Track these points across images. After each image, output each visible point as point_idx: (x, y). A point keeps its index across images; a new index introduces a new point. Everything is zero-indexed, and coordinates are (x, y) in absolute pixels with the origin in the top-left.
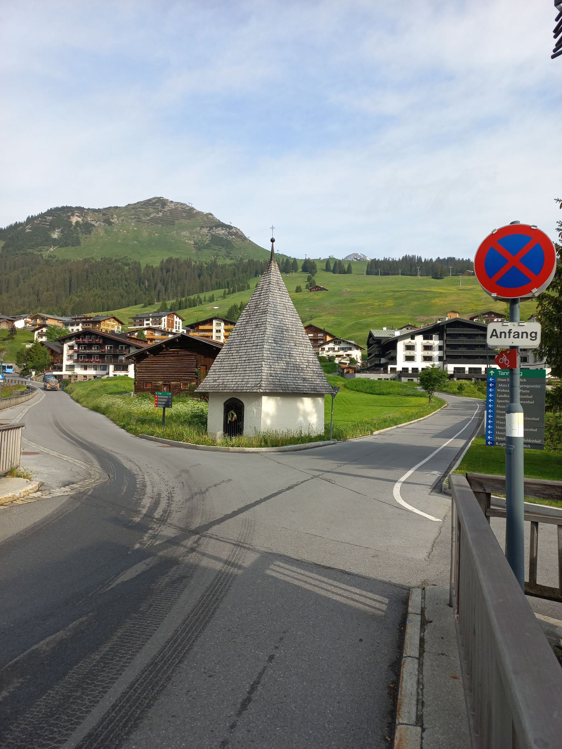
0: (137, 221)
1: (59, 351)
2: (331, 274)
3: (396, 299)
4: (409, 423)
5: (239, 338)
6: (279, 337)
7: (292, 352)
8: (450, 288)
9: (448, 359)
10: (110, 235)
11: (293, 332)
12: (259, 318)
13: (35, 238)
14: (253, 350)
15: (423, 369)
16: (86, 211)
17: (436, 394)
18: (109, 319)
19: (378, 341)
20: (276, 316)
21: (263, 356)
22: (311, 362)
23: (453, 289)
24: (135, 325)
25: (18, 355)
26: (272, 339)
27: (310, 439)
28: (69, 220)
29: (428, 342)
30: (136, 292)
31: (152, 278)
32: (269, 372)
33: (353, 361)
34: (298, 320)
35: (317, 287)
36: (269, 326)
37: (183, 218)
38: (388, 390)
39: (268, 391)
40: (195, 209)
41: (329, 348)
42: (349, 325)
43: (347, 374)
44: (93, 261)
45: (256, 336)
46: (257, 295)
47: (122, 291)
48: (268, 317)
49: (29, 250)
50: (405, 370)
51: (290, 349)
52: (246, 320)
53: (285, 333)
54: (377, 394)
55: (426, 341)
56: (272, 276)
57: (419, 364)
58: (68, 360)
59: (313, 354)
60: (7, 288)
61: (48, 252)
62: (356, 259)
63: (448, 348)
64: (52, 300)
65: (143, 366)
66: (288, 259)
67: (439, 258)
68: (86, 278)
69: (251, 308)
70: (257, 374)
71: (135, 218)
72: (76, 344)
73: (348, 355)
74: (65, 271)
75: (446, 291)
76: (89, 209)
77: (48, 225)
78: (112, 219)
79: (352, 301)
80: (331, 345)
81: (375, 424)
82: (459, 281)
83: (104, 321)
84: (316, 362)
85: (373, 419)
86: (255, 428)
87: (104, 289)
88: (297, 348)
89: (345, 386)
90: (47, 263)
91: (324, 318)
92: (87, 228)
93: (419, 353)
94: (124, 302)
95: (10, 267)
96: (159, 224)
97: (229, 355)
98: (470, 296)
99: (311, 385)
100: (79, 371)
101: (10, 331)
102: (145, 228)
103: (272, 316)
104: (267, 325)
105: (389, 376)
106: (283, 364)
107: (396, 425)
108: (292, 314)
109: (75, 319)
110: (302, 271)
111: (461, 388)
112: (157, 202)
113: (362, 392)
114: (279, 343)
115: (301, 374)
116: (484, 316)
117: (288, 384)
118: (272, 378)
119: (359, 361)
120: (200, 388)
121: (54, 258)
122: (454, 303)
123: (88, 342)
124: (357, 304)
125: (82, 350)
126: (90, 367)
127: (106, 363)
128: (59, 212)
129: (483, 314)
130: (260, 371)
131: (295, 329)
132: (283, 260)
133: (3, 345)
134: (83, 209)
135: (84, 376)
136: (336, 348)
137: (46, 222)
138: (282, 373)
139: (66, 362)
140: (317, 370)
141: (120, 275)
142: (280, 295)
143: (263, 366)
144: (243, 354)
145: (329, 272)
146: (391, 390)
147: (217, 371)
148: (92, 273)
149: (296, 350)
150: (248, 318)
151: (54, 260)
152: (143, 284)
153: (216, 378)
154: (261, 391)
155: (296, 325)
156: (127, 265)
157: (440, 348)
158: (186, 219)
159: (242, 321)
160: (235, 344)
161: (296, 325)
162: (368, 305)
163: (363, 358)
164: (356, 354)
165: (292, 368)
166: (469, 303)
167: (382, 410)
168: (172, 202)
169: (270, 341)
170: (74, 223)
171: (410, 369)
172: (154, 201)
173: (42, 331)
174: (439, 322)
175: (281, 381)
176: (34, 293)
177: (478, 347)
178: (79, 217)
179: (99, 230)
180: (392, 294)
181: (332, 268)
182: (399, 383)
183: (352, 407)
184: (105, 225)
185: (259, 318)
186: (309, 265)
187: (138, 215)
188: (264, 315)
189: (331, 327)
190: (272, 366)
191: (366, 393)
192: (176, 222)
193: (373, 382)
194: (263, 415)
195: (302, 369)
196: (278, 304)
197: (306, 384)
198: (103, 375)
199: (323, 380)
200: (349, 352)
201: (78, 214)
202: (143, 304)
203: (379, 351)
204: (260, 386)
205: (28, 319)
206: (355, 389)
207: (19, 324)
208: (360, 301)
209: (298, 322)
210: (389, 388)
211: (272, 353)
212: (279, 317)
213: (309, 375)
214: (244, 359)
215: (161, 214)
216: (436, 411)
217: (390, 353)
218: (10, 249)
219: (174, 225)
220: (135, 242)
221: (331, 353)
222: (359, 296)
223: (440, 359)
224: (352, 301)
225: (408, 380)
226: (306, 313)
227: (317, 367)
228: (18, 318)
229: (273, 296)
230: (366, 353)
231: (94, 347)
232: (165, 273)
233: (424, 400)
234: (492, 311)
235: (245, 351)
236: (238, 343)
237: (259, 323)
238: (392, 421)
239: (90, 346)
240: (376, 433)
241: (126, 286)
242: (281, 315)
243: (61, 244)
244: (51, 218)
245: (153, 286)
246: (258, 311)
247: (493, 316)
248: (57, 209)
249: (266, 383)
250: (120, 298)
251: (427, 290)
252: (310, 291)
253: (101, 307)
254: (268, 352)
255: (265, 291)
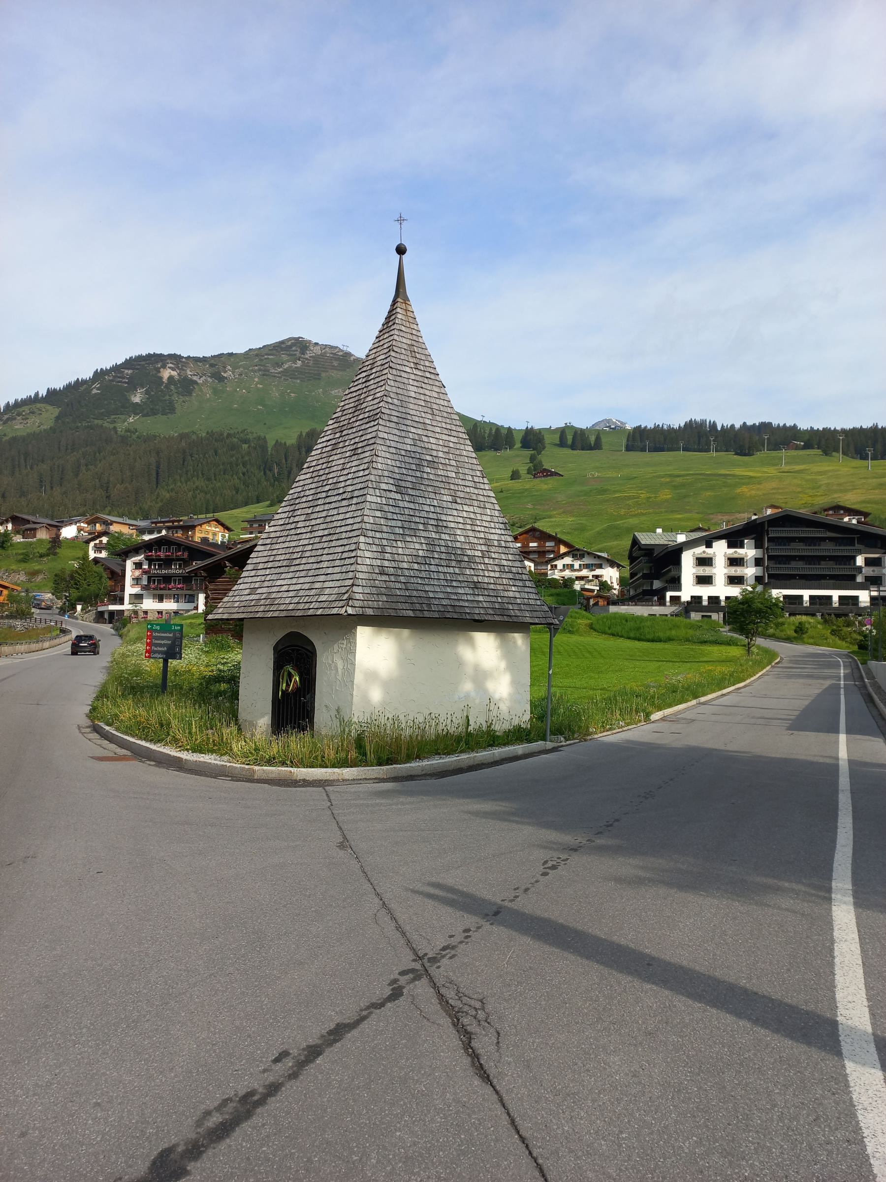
0: (264, 375)
1: (118, 570)
2: (567, 451)
3: (675, 487)
4: (720, 693)
5: (313, 486)
6: (409, 479)
7: (444, 518)
8: (765, 470)
9: (772, 580)
10: (221, 397)
11: (449, 468)
12: (360, 433)
13: (106, 402)
14: (342, 510)
15: (727, 598)
16: (184, 360)
17: (760, 641)
18: (208, 522)
19: (649, 550)
20: (404, 428)
21: (362, 521)
22: (496, 543)
23: (771, 471)
24: (251, 533)
25: (57, 578)
26: (391, 481)
27: (490, 739)
28: (159, 375)
29: (736, 552)
30: (259, 482)
31: (284, 461)
32: (379, 562)
33: (604, 586)
34: (462, 441)
35: (545, 470)
36: (384, 448)
37: (334, 368)
38: (668, 633)
39: (370, 612)
40: (353, 355)
41: (564, 565)
42: (597, 529)
43: (595, 607)
44: (194, 437)
45: (350, 476)
46: (360, 381)
47: (237, 481)
48: (380, 428)
49: (96, 422)
50: (697, 599)
51: (438, 510)
52: (333, 442)
53: (428, 470)
54: (648, 641)
55: (732, 551)
56: (396, 332)
57: (722, 590)
58: (132, 586)
59: (502, 526)
60: (61, 479)
61: (126, 423)
62: (609, 427)
63: (773, 562)
64: (128, 497)
65: (220, 587)
66: (498, 429)
67: (745, 423)
68: (182, 462)
69: (345, 412)
70: (344, 569)
71: (260, 370)
72: (146, 559)
73: (597, 577)
74: (150, 451)
75: (760, 475)
76: (189, 357)
77: (125, 383)
78: (225, 373)
79: (603, 491)
80: (568, 560)
81: (653, 697)
82: (781, 459)
83: (201, 525)
84: (508, 545)
85: (648, 686)
86: (338, 711)
87: (209, 479)
88: (459, 507)
89: (591, 627)
90: (124, 440)
91: (557, 519)
92: (186, 386)
93: (720, 571)
94: (240, 498)
95: (67, 447)
96: (297, 378)
97: (289, 527)
98: (800, 482)
99: (494, 599)
100: (149, 604)
101: (50, 542)
102: (275, 386)
103: (393, 425)
104: (379, 447)
105: (668, 609)
106: (417, 546)
107: (696, 697)
108: (449, 427)
109: (156, 523)
110: (521, 447)
111: (800, 630)
112: (293, 345)
113: (621, 636)
114: (410, 492)
115: (468, 572)
116: (826, 513)
117: (431, 595)
118: (384, 578)
119: (616, 586)
120: (220, 610)
121: (134, 434)
122: (773, 494)
123: (166, 556)
124: (610, 496)
125: (155, 569)
126: (169, 597)
127: (194, 591)
128: (143, 363)
129: (825, 510)
130: (352, 561)
131: (453, 463)
132: (491, 429)
133: (40, 564)
134: (180, 357)
135: (158, 612)
136: (577, 565)
137: (124, 378)
138: (416, 566)
139: (130, 589)
140: (510, 563)
141: (234, 458)
142: (418, 378)
143: (362, 546)
144: (318, 521)
145: (564, 449)
146: (674, 632)
147: (261, 566)
148: (191, 456)
149: (455, 513)
150: (338, 435)
151: (134, 436)
152: (270, 470)
153: (257, 585)
154: (350, 611)
155: (458, 452)
156: (246, 441)
157: (758, 562)
158: (339, 370)
159: (325, 444)
160: (304, 499)
161: (458, 452)
162: (629, 498)
163: (622, 581)
164: (611, 575)
165: (443, 556)
166: (799, 492)
167: (659, 667)
168: (316, 344)
169: (384, 486)
170: (165, 379)
171: (705, 598)
172: (290, 343)
173: (101, 542)
174: (754, 517)
175: (410, 586)
176: (102, 487)
177: (825, 560)
178: (173, 369)
179: (205, 389)
180: (668, 480)
181: (570, 442)
182: (688, 620)
183: (603, 662)
184: (213, 381)
185: (360, 433)
186: (532, 437)
187: (264, 366)
188: (372, 424)
189: (569, 533)
190: (388, 549)
191: (629, 638)
192: (323, 375)
193: (641, 619)
194: (358, 677)
195: (471, 559)
196: (412, 400)
197: (481, 598)
198: (188, 611)
199: (526, 590)
200: (598, 572)
201: (172, 366)
202: (269, 502)
203: (651, 568)
204: (350, 599)
205: (82, 525)
206: (609, 632)
207: (69, 532)
208: (615, 492)
209: (462, 447)
210: (670, 629)
211: (390, 516)
212: (413, 430)
213: (488, 575)
214: (320, 533)
215: (299, 363)
216: (765, 671)
217: (670, 571)
218: (67, 420)
219: (319, 379)
220: (259, 407)
221: (567, 573)
222: (614, 484)
223: (759, 579)
224: (603, 491)
225: (703, 616)
226: (528, 512)
227: (510, 557)
228: (67, 522)
229: (398, 379)
230: (627, 574)
231: (175, 565)
232: (304, 453)
233: (735, 652)
234: (841, 504)
235: (324, 514)
236: (310, 498)
237: (360, 445)
238: (687, 689)
239: (167, 563)
240: (656, 716)
241: (244, 474)
242: (420, 426)
243: (145, 412)
244: (130, 372)
245: (286, 473)
246: (361, 417)
247: (842, 512)
248: (140, 358)
249: (367, 590)
250: (234, 492)
251: (728, 473)
252: (534, 477)
253: (204, 506)
254: (378, 514)
255: (379, 369)
